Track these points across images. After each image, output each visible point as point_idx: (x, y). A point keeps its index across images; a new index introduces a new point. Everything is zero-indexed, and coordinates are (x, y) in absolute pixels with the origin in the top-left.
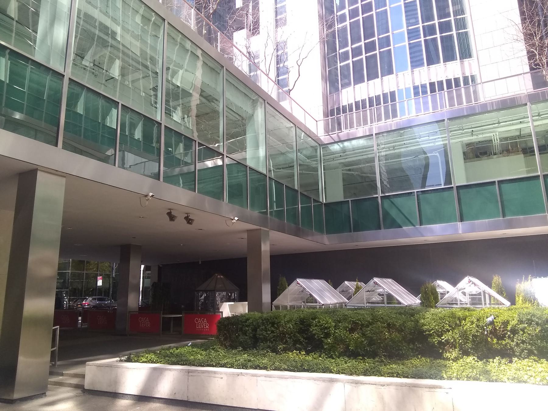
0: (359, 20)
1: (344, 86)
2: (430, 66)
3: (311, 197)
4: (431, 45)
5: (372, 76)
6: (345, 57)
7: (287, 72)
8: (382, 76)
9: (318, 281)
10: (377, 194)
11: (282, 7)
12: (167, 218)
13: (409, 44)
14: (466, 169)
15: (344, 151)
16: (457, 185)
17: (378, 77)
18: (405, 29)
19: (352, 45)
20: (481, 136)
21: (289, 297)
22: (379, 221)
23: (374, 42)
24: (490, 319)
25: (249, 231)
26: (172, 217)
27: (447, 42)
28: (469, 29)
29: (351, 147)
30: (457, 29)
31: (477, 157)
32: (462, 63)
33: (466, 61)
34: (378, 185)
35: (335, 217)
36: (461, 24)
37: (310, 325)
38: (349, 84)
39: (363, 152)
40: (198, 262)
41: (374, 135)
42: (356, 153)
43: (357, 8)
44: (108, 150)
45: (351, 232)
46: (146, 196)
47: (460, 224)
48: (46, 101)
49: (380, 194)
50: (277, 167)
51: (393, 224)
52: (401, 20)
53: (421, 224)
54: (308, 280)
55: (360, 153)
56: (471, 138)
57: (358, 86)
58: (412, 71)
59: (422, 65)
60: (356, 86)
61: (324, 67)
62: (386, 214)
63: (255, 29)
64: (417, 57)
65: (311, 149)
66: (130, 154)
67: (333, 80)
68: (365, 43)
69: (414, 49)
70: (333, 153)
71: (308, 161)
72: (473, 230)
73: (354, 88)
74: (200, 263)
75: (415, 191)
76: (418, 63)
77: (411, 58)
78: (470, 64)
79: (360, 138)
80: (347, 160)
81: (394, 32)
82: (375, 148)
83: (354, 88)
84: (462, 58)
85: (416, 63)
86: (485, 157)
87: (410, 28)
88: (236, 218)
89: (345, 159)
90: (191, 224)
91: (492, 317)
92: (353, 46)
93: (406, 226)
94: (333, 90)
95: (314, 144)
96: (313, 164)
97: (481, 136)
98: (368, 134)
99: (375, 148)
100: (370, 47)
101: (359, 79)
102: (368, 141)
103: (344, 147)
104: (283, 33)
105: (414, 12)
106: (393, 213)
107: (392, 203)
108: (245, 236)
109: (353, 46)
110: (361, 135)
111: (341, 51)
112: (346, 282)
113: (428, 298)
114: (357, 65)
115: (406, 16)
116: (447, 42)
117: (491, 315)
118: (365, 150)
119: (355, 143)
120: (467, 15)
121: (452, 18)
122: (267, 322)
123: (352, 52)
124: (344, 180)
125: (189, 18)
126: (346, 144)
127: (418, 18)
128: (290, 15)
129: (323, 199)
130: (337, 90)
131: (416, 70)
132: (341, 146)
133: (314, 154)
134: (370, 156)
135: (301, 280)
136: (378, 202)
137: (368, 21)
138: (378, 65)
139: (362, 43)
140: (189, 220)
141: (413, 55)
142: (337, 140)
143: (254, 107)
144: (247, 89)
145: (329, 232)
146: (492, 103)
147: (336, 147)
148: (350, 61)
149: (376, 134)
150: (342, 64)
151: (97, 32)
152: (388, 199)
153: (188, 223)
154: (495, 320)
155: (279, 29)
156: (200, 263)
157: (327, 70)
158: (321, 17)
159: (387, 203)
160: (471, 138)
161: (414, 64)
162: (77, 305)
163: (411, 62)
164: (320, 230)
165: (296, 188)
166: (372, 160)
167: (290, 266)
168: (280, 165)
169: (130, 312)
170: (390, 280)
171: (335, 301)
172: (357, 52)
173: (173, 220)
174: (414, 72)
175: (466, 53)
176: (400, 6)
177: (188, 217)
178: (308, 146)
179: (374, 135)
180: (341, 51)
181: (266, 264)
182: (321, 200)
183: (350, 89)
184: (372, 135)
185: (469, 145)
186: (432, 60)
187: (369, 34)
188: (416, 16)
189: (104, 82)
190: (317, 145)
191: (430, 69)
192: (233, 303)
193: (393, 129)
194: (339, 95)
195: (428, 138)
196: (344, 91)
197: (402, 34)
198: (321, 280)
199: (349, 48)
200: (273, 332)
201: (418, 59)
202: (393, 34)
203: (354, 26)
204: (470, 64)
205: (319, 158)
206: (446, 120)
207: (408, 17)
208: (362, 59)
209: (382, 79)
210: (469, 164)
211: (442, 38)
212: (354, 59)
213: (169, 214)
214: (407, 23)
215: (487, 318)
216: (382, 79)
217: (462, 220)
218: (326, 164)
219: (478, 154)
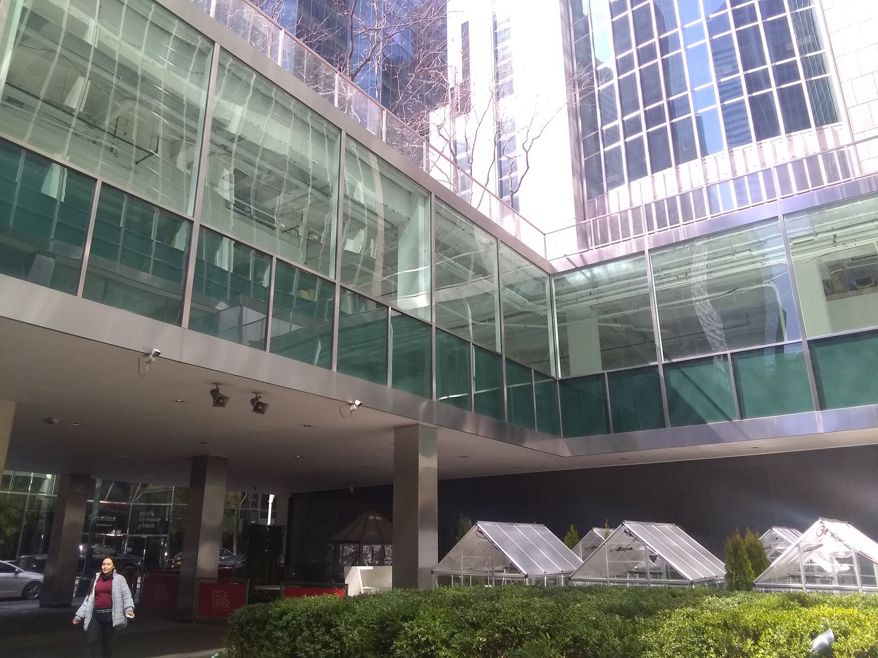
0: (634, 74)
1: (611, 185)
2: (763, 141)
3: (531, 366)
4: (761, 107)
5: (660, 163)
6: (612, 137)
7: (513, 168)
8: (677, 163)
9: (530, 526)
10: (656, 360)
11: (506, 66)
12: (211, 400)
13: (724, 108)
14: (831, 313)
15: (594, 283)
16: (808, 338)
17: (670, 166)
18: (714, 82)
19: (623, 116)
20: (851, 245)
21: (465, 557)
22: (662, 412)
23: (660, 108)
24: (822, 639)
25: (397, 429)
26: (219, 399)
27: (792, 99)
28: (831, 74)
29: (606, 278)
30: (808, 75)
31: (853, 288)
32: (820, 132)
33: (828, 129)
34: (657, 344)
35: (579, 405)
36: (816, 66)
37: (395, 635)
38: (620, 182)
39: (629, 284)
40: (349, 490)
41: (647, 252)
42: (614, 288)
43: (630, 56)
44: (217, 304)
45: (609, 432)
46: (147, 355)
47: (818, 414)
48: (123, 231)
49: (661, 360)
50: (480, 319)
51: (684, 415)
52: (708, 69)
53: (742, 416)
54: (505, 525)
55: (623, 286)
56: (832, 249)
57: (635, 184)
58: (731, 152)
59: (748, 140)
60: (632, 183)
61: (576, 156)
62: (675, 397)
63: (464, 106)
64: (738, 128)
65: (534, 284)
66: (249, 310)
67: (594, 174)
68: (645, 112)
69: (732, 114)
70: (574, 290)
71: (528, 304)
72: (847, 424)
73: (629, 186)
74: (352, 490)
75: (728, 352)
76: (742, 138)
77: (725, 125)
78: (835, 133)
79: (621, 261)
80: (601, 301)
81: (696, 89)
82: (650, 277)
83: (629, 186)
84: (819, 123)
85: (737, 137)
86: (867, 289)
87: (722, 80)
88: (358, 402)
89: (597, 298)
90: (261, 412)
91: (830, 634)
92: (626, 118)
93: (715, 419)
94: (594, 192)
95: (540, 274)
96: (539, 309)
97: (851, 245)
98: (635, 251)
99: (650, 277)
100: (654, 117)
101: (637, 171)
102: (637, 264)
103: (593, 276)
104: (508, 107)
105: (731, 53)
106: (687, 394)
107: (686, 376)
108: (391, 437)
109: (626, 118)
110: (623, 254)
111: (604, 128)
112: (596, 530)
113: (741, 566)
114: (633, 150)
115: (715, 60)
116: (792, 99)
117: (826, 628)
118: (632, 280)
119: (611, 267)
120: (825, 50)
121: (797, 58)
122: (317, 622)
123: (623, 124)
124: (604, 341)
125: (280, 48)
126: (597, 270)
127: (736, 61)
128: (517, 77)
129: (557, 372)
130: (601, 191)
131: (738, 150)
132: (588, 274)
133: (541, 292)
134: (642, 291)
135: (487, 524)
136: (658, 375)
137: (649, 76)
138: (671, 145)
139: (641, 112)
140: (258, 406)
141: (731, 126)
142: (579, 264)
143: (412, 208)
144: (392, 170)
145: (569, 433)
146: (869, 180)
147: (578, 278)
148: (621, 143)
149: (650, 250)
150: (607, 149)
151: (114, 80)
152: (678, 368)
153: (256, 410)
154: (835, 645)
155: (501, 100)
156: (352, 490)
157: (583, 160)
158: (569, 75)
159: (675, 377)
160: (832, 249)
161: (733, 140)
162: (176, 561)
163: (728, 137)
164: (552, 430)
165: (498, 350)
166: (645, 300)
167: (475, 495)
168: (484, 315)
169: (199, 578)
170: (668, 527)
171: (557, 568)
172: (632, 127)
173: (223, 405)
174: (734, 153)
175: (827, 114)
176: (705, 44)
177: (257, 398)
178: (528, 278)
179: (647, 252)
180: (604, 128)
181: (428, 493)
182: (553, 374)
183: (623, 189)
184: (643, 253)
185: (834, 266)
186: (766, 129)
187: (652, 94)
188: (732, 59)
189: (133, 165)
190: (544, 275)
191: (763, 145)
192: (371, 568)
193: (682, 239)
194: (604, 200)
195: (748, 253)
196: (613, 193)
197: (710, 90)
198: (537, 526)
199: (618, 122)
200: (326, 645)
201: (741, 130)
202: (693, 92)
203: (626, 86)
204: (835, 133)
205: (548, 299)
206: (781, 217)
207: (719, 62)
208: (641, 138)
209: (677, 169)
210: (838, 303)
211: (781, 92)
212: (628, 139)
213: (214, 392)
214: (716, 72)
215: (813, 636)
216: (677, 169)
217: (822, 406)
218: (564, 309)
219: (854, 283)
